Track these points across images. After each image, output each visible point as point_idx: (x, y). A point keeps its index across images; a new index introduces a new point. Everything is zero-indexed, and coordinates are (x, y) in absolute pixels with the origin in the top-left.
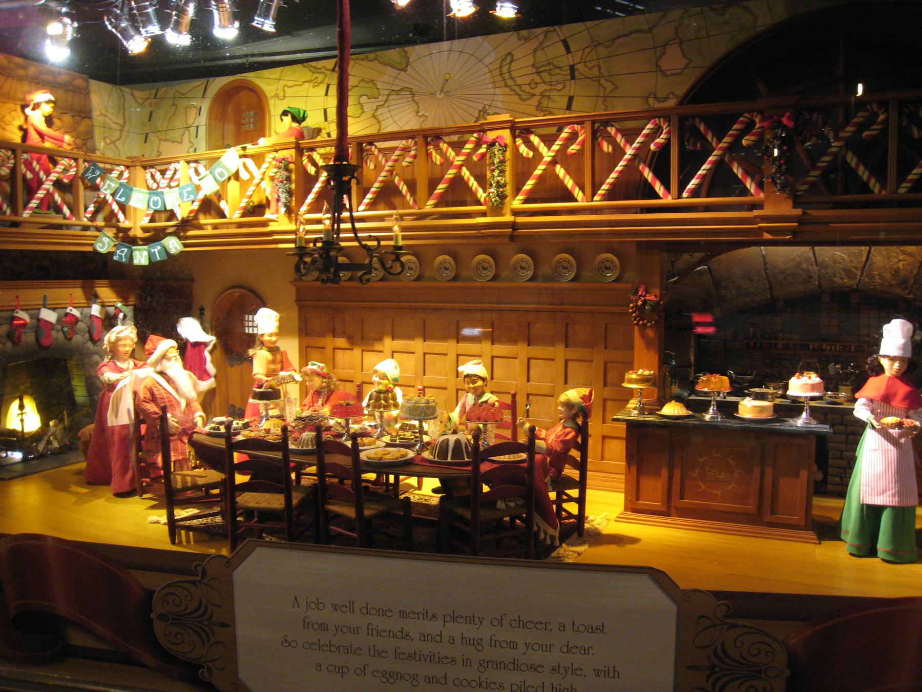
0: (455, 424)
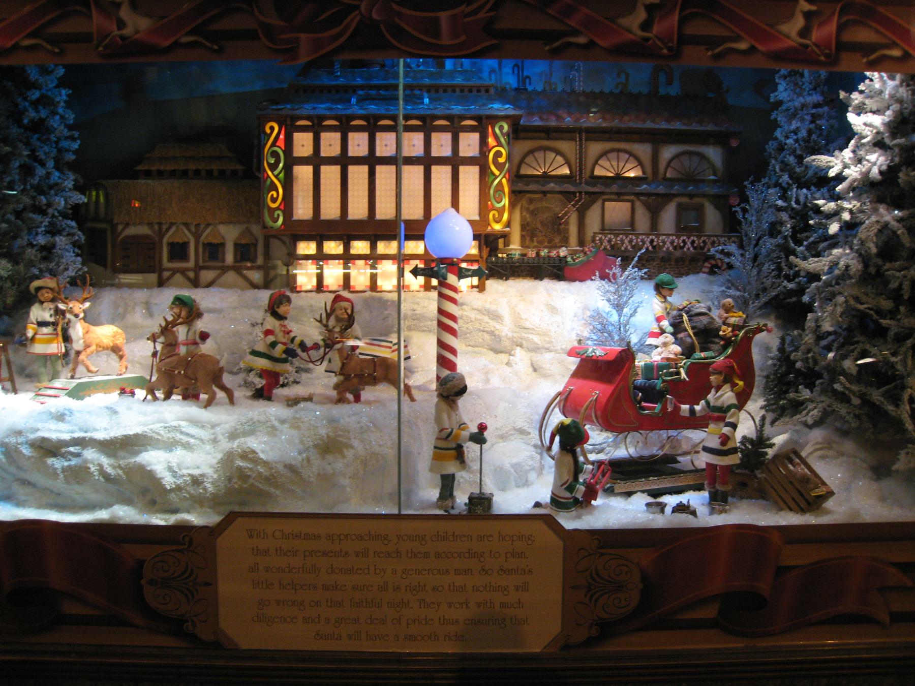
0: (462, 426)
